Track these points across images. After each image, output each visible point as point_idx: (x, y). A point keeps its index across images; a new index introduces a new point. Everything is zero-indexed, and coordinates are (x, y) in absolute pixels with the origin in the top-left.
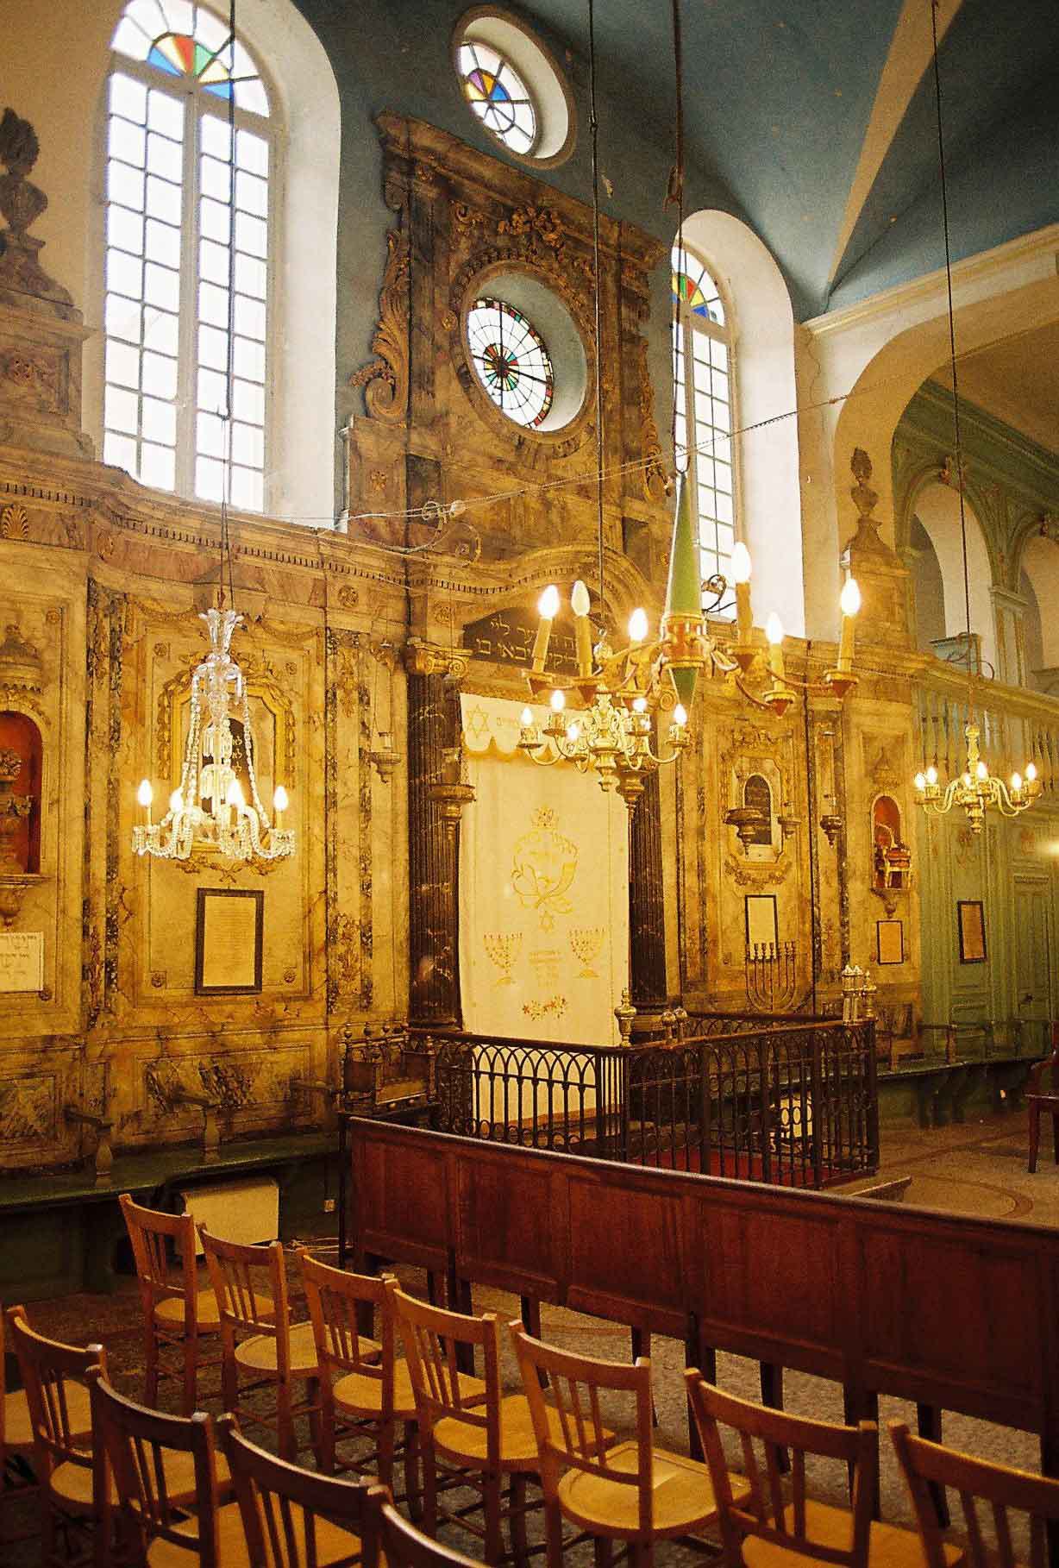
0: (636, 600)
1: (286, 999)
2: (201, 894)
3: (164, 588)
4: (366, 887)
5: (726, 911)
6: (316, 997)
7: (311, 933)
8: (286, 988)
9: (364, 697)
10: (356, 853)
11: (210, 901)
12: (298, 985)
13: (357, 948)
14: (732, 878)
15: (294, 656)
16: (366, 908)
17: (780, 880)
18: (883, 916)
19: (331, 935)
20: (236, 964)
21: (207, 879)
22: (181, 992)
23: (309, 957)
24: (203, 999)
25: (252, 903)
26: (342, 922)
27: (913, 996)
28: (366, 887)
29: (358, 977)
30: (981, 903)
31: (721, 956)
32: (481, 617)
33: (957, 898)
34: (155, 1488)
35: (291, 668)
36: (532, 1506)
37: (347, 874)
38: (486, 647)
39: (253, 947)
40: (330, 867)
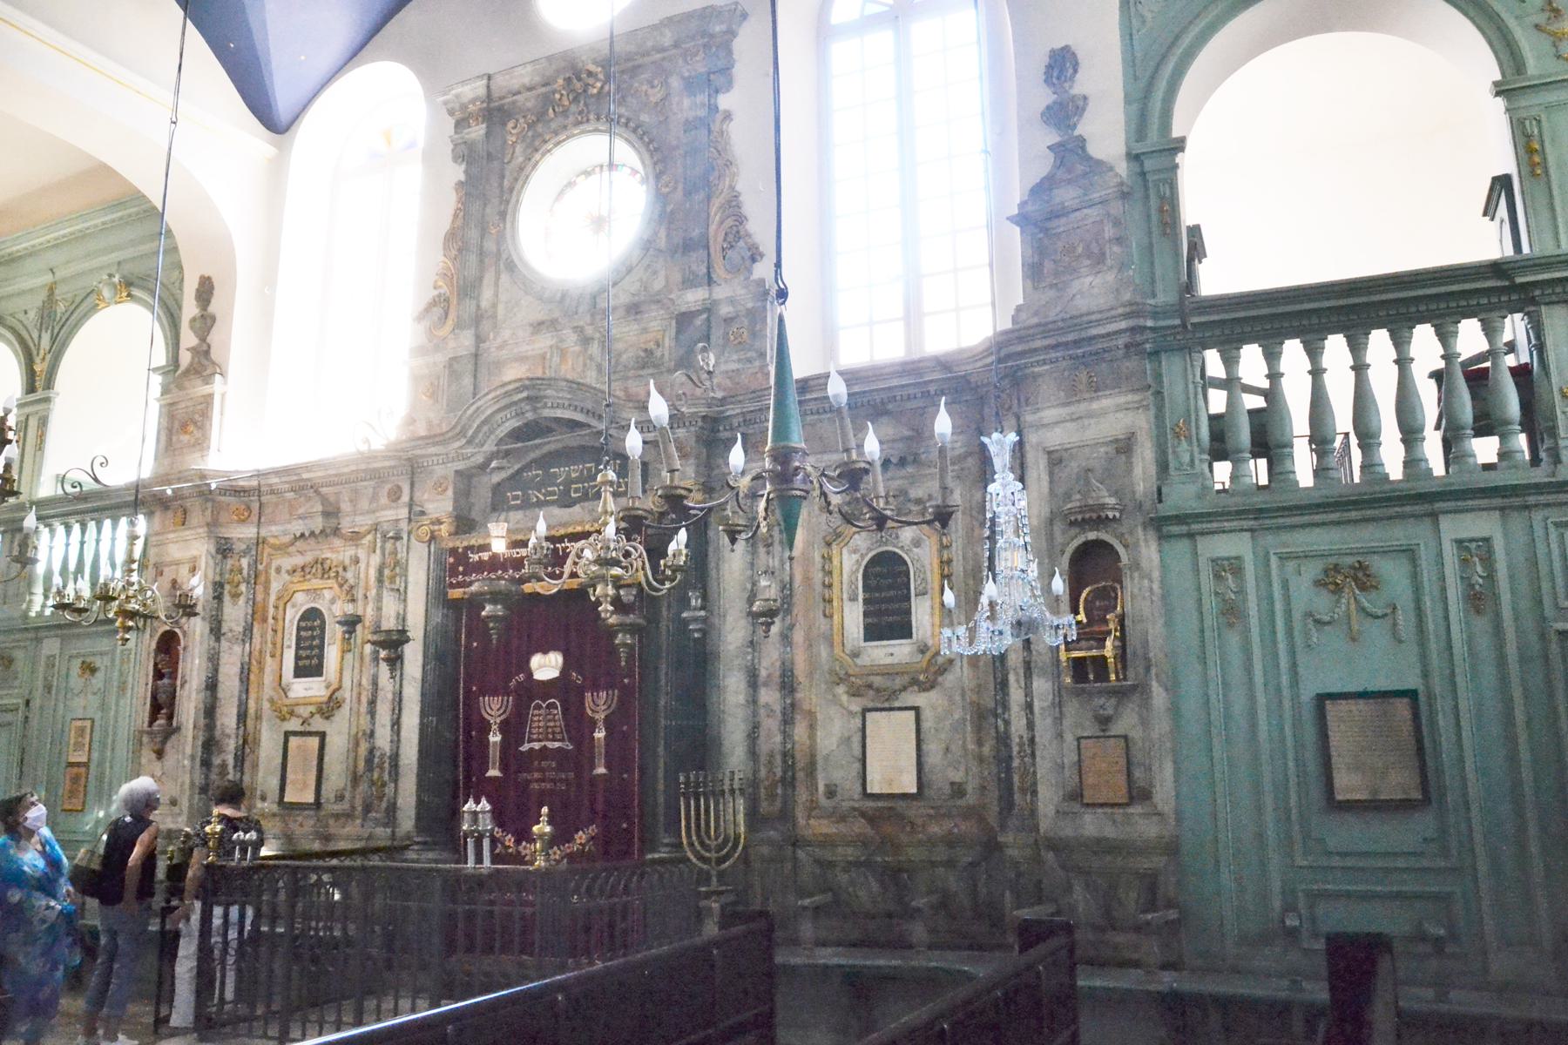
1: (337, 816)
2: (287, 734)
3: (280, 528)
5: (830, 730)
8: (338, 808)
10: (390, 696)
11: (293, 741)
12: (345, 806)
13: (386, 777)
14: (841, 690)
17: (928, 686)
18: (1090, 729)
20: (305, 785)
21: (294, 725)
23: (355, 779)
26: (378, 754)
27: (1158, 862)
30: (1412, 694)
31: (821, 788)
33: (1310, 688)
38: (516, 498)
40: (372, 713)
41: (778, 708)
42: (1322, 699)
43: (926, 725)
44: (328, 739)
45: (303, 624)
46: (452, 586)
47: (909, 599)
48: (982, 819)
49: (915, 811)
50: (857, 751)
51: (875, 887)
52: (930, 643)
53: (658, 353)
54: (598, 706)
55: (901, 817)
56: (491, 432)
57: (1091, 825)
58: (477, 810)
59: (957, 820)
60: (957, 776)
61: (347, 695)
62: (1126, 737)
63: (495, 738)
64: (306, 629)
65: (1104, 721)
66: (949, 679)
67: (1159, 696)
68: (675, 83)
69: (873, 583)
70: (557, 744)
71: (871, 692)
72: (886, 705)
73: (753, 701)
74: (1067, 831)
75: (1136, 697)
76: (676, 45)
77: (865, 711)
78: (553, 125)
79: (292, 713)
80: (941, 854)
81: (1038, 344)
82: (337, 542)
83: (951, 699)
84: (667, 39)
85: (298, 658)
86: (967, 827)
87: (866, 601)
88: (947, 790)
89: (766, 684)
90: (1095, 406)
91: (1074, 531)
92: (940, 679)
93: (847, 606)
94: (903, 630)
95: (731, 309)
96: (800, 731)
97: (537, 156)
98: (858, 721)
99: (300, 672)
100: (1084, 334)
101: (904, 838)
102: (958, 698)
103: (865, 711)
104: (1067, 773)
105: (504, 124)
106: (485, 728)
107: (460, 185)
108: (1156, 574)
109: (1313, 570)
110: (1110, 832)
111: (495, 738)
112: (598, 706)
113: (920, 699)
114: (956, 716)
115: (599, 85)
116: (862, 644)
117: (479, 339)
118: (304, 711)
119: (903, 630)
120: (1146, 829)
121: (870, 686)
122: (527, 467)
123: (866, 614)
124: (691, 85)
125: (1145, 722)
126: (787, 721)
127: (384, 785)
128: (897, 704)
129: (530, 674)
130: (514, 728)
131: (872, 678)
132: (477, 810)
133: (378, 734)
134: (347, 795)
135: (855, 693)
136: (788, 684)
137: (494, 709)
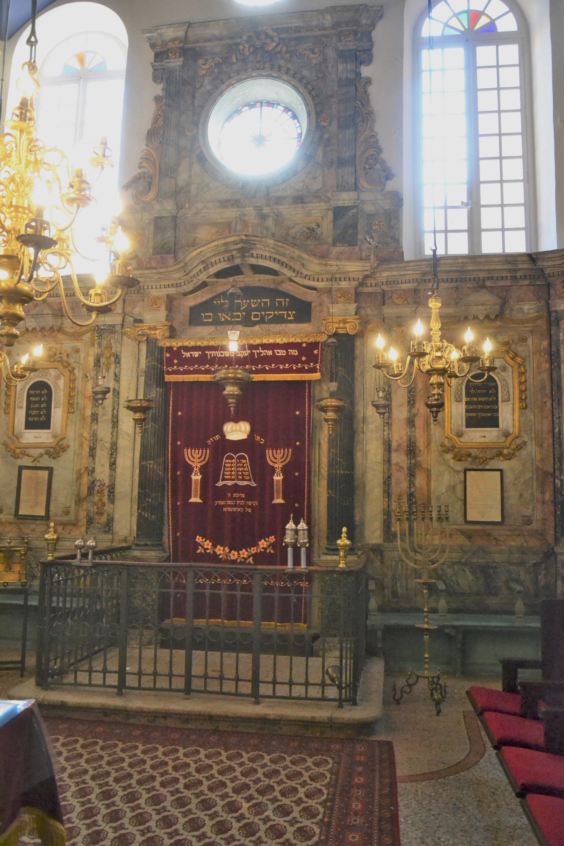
0: (413, 316)
2: (21, 468)
4: (113, 465)
6: (80, 523)
7: (79, 489)
8: (65, 519)
9: (118, 360)
10: (108, 445)
11: (25, 472)
13: (105, 499)
14: (449, 456)
15: (78, 344)
16: (112, 477)
17: (509, 457)
19: (91, 489)
21: (26, 461)
22: (10, 516)
23: (79, 501)
24: (21, 521)
25: (46, 473)
28: (113, 465)
29: (105, 515)
32: (204, 299)
34: (348, 663)
35: (77, 351)
36: (359, 786)
37: (102, 456)
39: (15, 495)
41: (405, 465)
43: (506, 481)
44: (55, 473)
45: (32, 392)
46: (169, 373)
47: (496, 402)
49: (497, 531)
50: (460, 494)
51: (471, 577)
52: (511, 431)
53: (319, 231)
54: (277, 459)
55: (489, 535)
56: (205, 269)
60: (528, 512)
61: (71, 443)
63: (196, 477)
64: (35, 395)
68: (331, 53)
69: (472, 391)
70: (245, 483)
71: (470, 459)
72: (480, 467)
73: (388, 461)
76: (334, 27)
77: (466, 470)
78: (235, 67)
79: (24, 454)
80: (516, 557)
82: (60, 336)
84: (328, 20)
85: (28, 415)
86: (533, 543)
87: (467, 403)
89: (397, 450)
92: (517, 453)
93: (454, 405)
94: (493, 422)
95: (372, 208)
96: (420, 480)
97: (224, 86)
98: (462, 476)
99: (471, 423)
102: (528, 464)
103: (466, 470)
105: (196, 61)
106: (189, 470)
107: (157, 99)
111: (196, 477)
112: (277, 459)
113: (503, 465)
114: (528, 476)
115: (274, 45)
116: (464, 429)
117: (179, 207)
118: (35, 452)
119: (493, 422)
121: (469, 455)
122: (218, 297)
123: (467, 411)
124: (343, 56)
126: (412, 475)
127: (104, 505)
128: (488, 467)
129: (223, 436)
130: (211, 471)
131: (471, 450)
133: (98, 469)
134: (72, 510)
135: (459, 458)
136: (412, 450)
137: (195, 458)
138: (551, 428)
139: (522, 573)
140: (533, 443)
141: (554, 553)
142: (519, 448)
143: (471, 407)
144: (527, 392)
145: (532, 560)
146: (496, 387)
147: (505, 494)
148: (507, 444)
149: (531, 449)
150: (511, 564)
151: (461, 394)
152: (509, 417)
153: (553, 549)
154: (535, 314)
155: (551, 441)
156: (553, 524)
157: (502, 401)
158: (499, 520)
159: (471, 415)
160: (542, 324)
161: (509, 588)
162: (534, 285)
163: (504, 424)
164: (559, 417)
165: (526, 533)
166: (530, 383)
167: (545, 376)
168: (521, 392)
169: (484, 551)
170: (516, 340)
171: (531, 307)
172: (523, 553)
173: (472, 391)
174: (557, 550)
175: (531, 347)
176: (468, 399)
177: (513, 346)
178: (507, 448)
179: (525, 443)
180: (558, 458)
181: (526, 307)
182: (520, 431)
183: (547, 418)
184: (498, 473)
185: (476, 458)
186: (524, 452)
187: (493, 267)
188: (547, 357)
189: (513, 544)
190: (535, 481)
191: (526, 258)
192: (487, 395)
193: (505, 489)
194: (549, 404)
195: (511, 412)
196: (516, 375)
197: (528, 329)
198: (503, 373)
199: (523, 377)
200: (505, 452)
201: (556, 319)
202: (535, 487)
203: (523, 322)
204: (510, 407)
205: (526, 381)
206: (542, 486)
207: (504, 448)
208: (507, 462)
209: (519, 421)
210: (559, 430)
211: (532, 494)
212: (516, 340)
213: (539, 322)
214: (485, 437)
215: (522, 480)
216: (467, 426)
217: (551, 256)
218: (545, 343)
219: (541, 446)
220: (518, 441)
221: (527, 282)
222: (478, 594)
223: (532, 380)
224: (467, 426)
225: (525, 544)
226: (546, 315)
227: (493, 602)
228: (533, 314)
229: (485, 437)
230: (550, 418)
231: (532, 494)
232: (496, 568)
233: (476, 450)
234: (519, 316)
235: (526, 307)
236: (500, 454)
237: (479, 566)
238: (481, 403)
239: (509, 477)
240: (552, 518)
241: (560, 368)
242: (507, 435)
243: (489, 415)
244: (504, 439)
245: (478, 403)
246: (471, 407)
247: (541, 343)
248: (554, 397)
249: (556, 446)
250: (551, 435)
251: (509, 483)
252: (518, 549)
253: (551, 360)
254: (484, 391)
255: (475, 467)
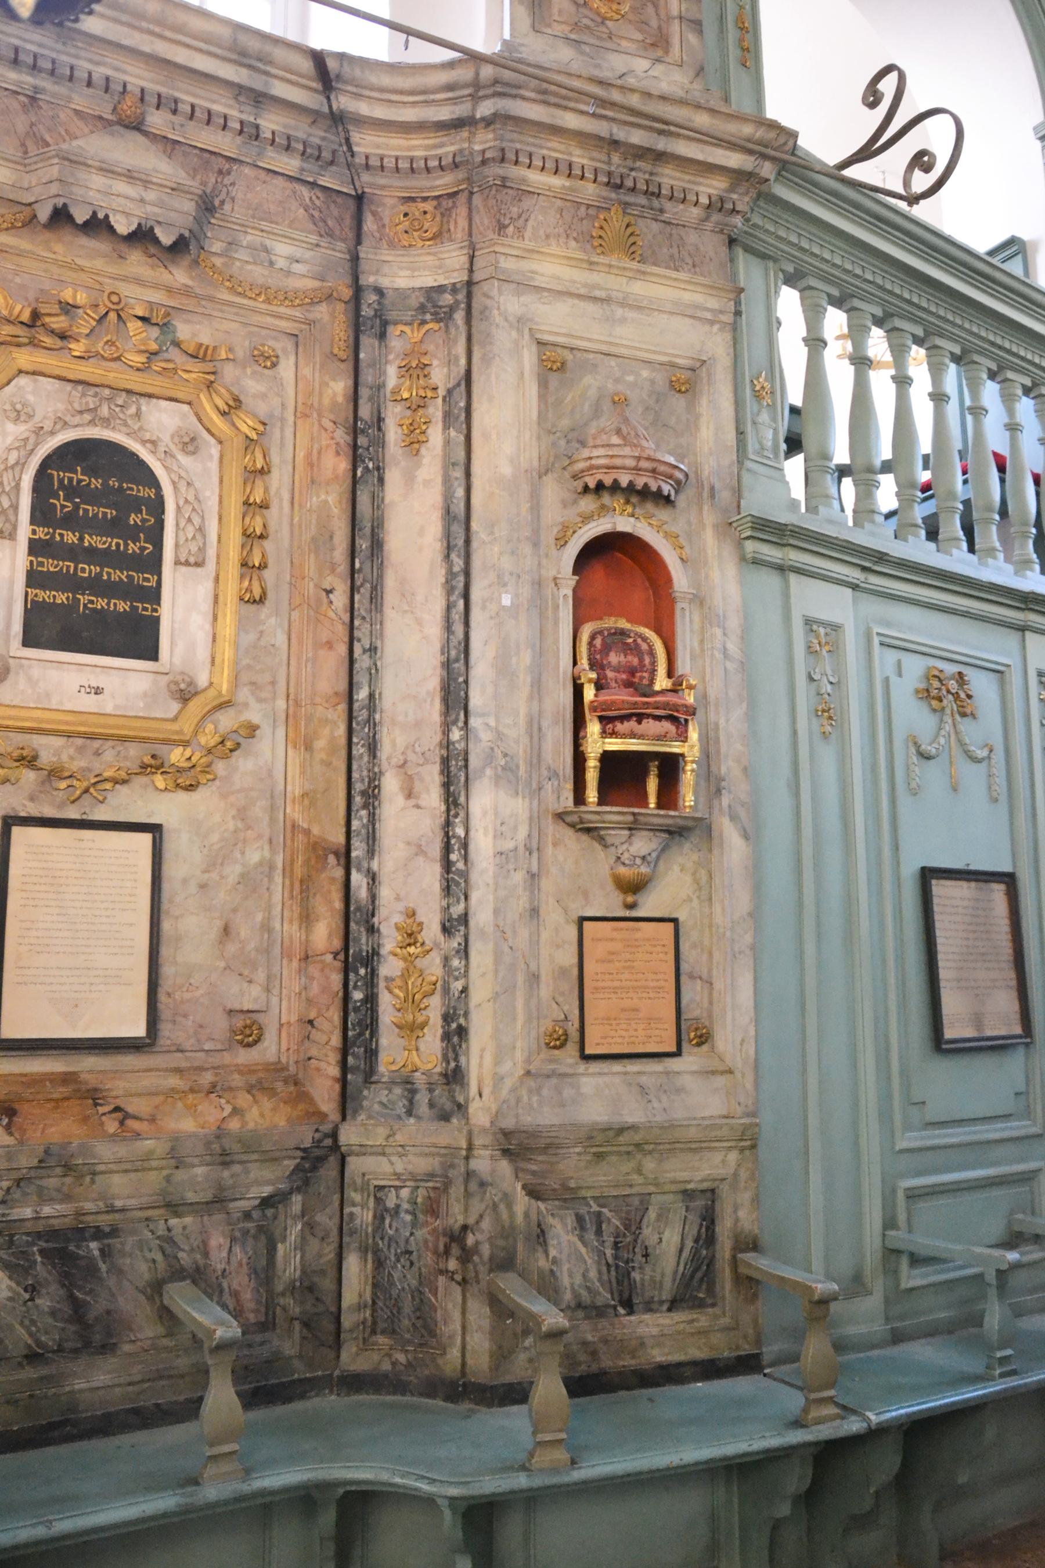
18: (607, 901)
30: (1009, 880)
42: (928, 875)
43: (174, 870)
47: (155, 563)
48: (302, 1096)
49: (128, 1080)
52: (202, 680)
55: (94, 1096)
57: (598, 1097)
58: (133, 519)
59: (243, 1099)
60: (250, 997)
62: (675, 921)
65: (633, 887)
66: (244, 767)
67: (734, 846)
71: (29, 776)
74: (542, 1115)
75: (694, 838)
80: (197, 1179)
81: (571, 121)
83: (242, 813)
86: (263, 1116)
87: (35, 548)
88: (220, 1026)
90: (639, 288)
91: (588, 504)
92: (220, 767)
94: (138, 638)
100: (661, 144)
101: (106, 1151)
102: (259, 811)
104: (545, 992)
108: (734, 623)
109: (915, 667)
110: (633, 1113)
113: (164, 807)
114: (254, 856)
119: (138, 638)
120: (696, 1095)
121: (29, 760)
123: (34, 579)
125: (706, 891)
128: (101, 814)
131: (38, 741)
132: (133, 519)
138: (343, 686)
139: (217, 1241)
140: (281, 732)
141: (336, 1147)
142: (228, 747)
143: (50, 565)
144: (267, 544)
145: (260, 1181)
146: (158, 507)
147: (166, 926)
148: (186, 726)
149: (271, 752)
150: (174, 1208)
151: (15, 507)
152: (198, 626)
153: (334, 1135)
154: (311, 284)
155: (341, 730)
156: (336, 1040)
157: (177, 562)
158: (138, 1029)
159: (43, 595)
160: (333, 321)
161: (167, 1316)
162: (313, 185)
163: (180, 649)
164: (372, 650)
165: (237, 1080)
166: (278, 517)
167: (332, 499)
168: (250, 538)
169: (68, 1168)
170: (240, 354)
171: (298, 253)
172: (225, 1159)
173: (61, 504)
174: (349, 1135)
175: (291, 391)
176: (41, 533)
177: (229, 372)
178: (186, 744)
179: (252, 730)
180: (363, 793)
181: (282, 249)
182: (236, 681)
183: (330, 645)
184: (145, 839)
185: (55, 773)
186: (244, 765)
187: (181, 56)
188: (342, 436)
189: (188, 1125)
190: (278, 879)
191: (306, 65)
192: (115, 527)
193: (165, 905)
194: (340, 599)
195: (206, 606)
196: (235, 475)
197: (284, 324)
198: (182, 458)
199: (259, 483)
200: (176, 756)
201: (379, 314)
202: (277, 897)
203: (268, 294)
204: (204, 589)
205: (264, 506)
206: (304, 890)
207: (176, 743)
208: (182, 796)
209: (236, 646)
210: (371, 696)
211: (266, 928)
212: (240, 354)
213: (322, 311)
214: (98, 691)
215: (233, 872)
216: (29, 641)
217: (386, 80)
218: (339, 387)
219: (309, 747)
220: (226, 721)
221: (291, 164)
222: (33, 1357)
223: (286, 504)
224: (29, 641)
225: (234, 1125)
226: (347, 293)
227: (96, 1381)
228: (302, 279)
229: (98, 691)
230: (342, 649)
231: (266, 928)
232: (114, 1232)
233: (59, 742)
234: (258, 273)
235: (282, 249)
236: (154, 766)
237: (39, 1235)
238: (92, 555)
239: (184, 859)
240: (335, 1015)
241: (381, 480)
242: (185, 693)
243: (123, 606)
244: (175, 707)
245: (73, 553)
246: (50, 565)
247: (324, 384)
248: (359, 579)
249: (359, 750)
250: (343, 707)
251: (185, 881)
252: (208, 1144)
253: (355, 447)
254: (111, 513)
255: (49, 812)
